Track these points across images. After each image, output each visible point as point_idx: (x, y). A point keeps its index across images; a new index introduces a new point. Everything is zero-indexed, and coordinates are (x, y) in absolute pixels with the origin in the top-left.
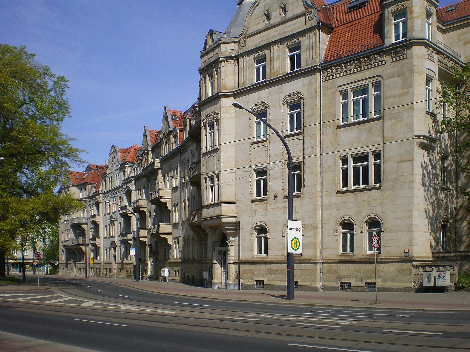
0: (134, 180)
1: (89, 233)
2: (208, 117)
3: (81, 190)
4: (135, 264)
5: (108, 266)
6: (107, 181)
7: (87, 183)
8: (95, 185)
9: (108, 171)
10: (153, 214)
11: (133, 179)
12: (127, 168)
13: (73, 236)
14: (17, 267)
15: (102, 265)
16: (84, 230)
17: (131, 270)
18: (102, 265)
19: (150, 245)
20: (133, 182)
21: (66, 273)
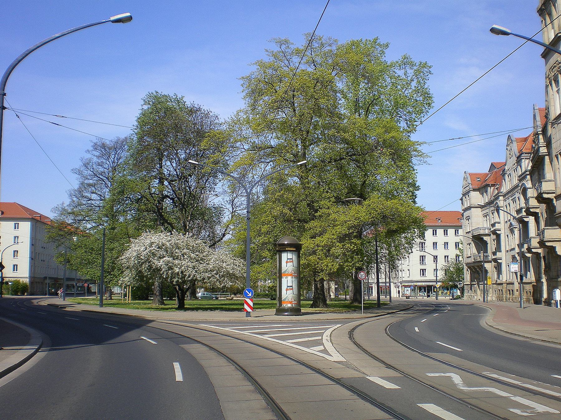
0: (530, 174)
1: (491, 246)
2: (553, 69)
3: (482, 194)
4: (535, 284)
5: (510, 287)
6: (506, 179)
7: (488, 185)
8: (497, 186)
9: (506, 168)
10: (545, 215)
11: (528, 173)
12: (523, 160)
13: (475, 251)
14: (425, 291)
15: (505, 285)
16: (486, 242)
17: (530, 292)
18: (505, 285)
19: (544, 257)
20: (528, 177)
21: (471, 297)
